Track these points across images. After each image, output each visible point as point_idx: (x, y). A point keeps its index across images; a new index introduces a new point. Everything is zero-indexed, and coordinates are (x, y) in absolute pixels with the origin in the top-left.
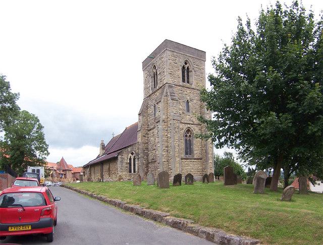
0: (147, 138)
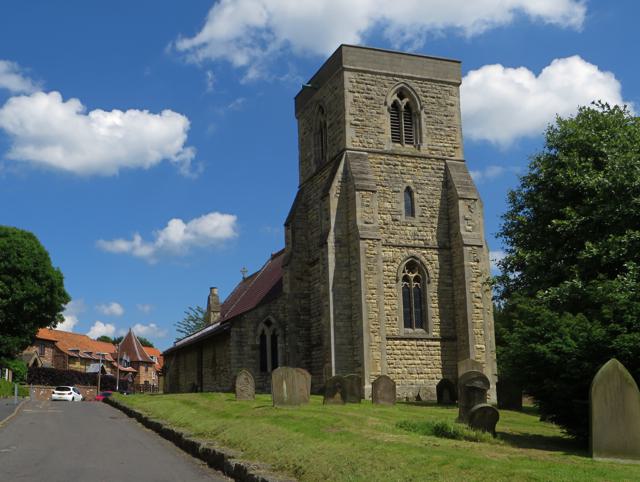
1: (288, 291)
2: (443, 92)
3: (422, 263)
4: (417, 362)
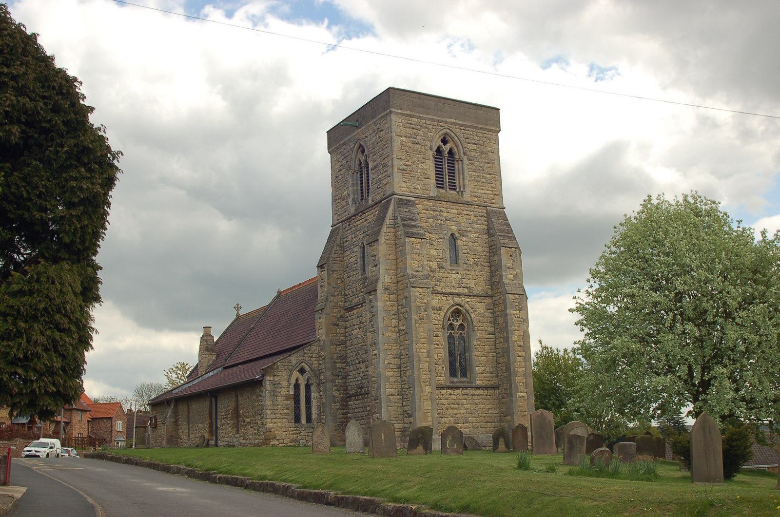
0: (342, 330)
1: (324, 338)
2: (484, 139)
3: (466, 310)
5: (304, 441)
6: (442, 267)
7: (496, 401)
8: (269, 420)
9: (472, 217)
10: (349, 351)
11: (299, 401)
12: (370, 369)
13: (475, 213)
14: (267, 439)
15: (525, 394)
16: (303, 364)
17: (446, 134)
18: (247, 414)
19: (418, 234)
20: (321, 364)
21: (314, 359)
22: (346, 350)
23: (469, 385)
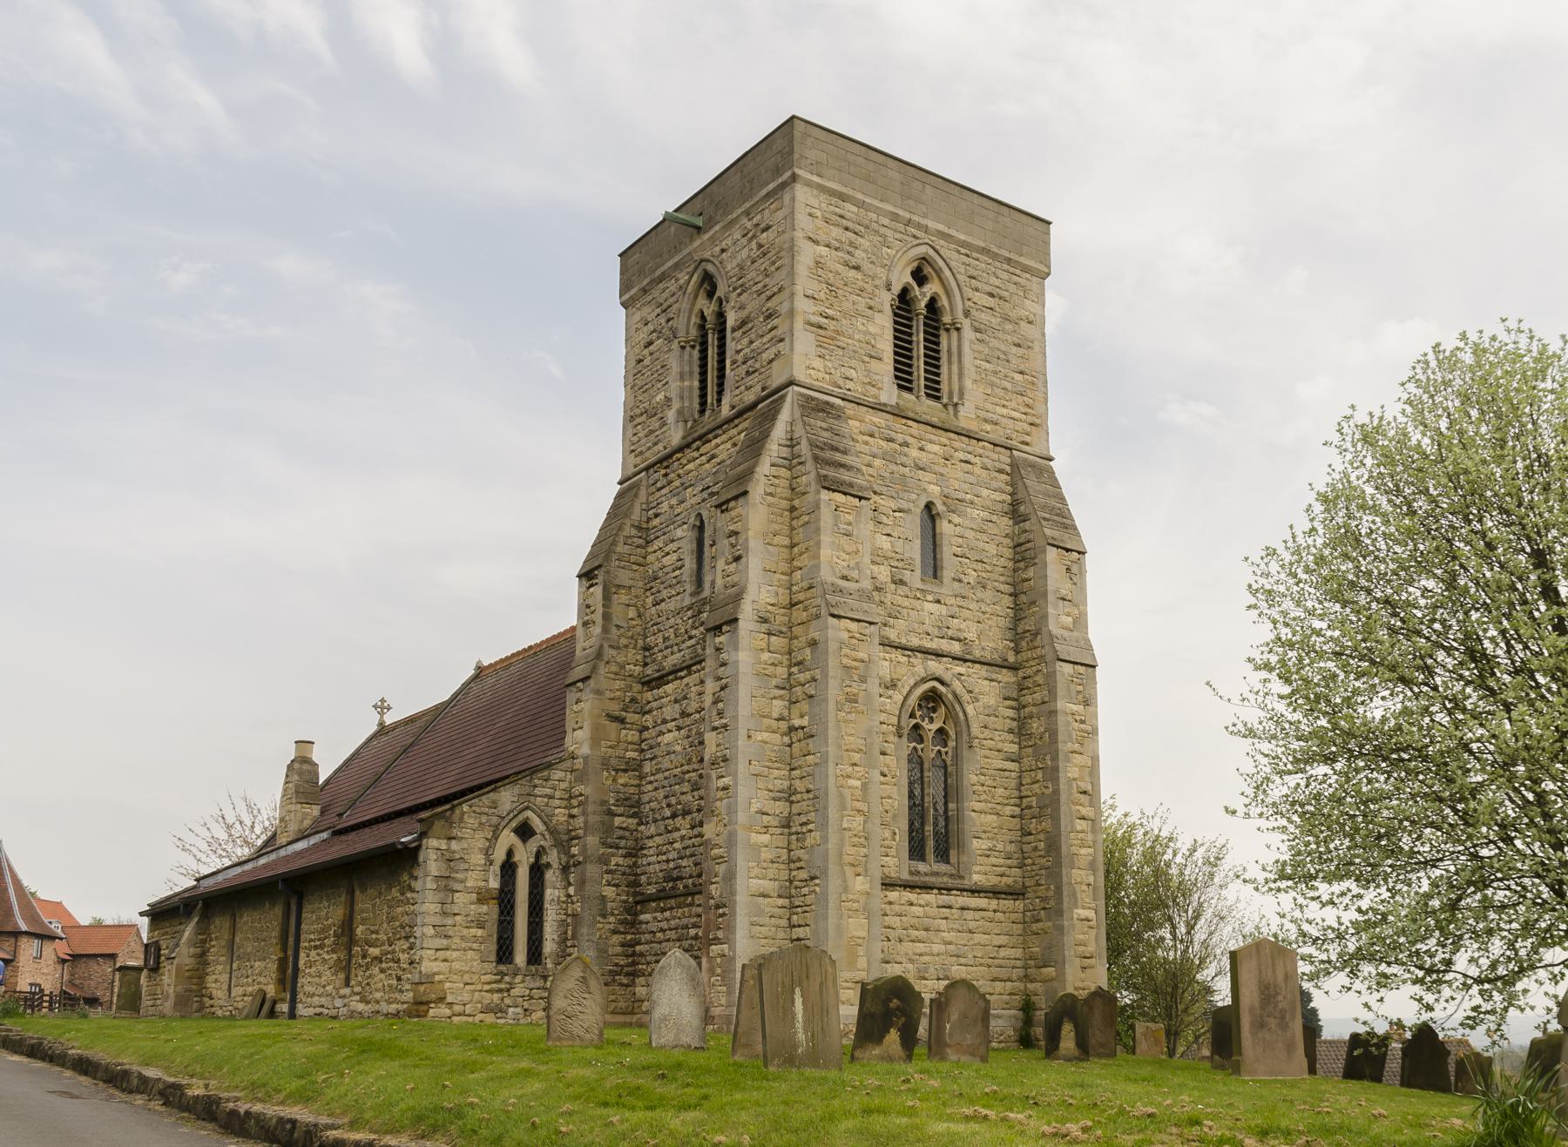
0: (632, 735)
1: (585, 750)
2: (1012, 288)
3: (955, 695)
4: (936, 948)
5: (519, 1010)
6: (902, 582)
7: (1018, 928)
8: (429, 952)
9: (977, 470)
10: (650, 787)
11: (512, 907)
12: (709, 830)
13: (985, 460)
14: (421, 1003)
15: (1091, 914)
16: (529, 813)
17: (924, 258)
18: (374, 936)
19: (851, 485)
20: (573, 816)
21: (557, 802)
22: (638, 786)
23: (957, 883)
